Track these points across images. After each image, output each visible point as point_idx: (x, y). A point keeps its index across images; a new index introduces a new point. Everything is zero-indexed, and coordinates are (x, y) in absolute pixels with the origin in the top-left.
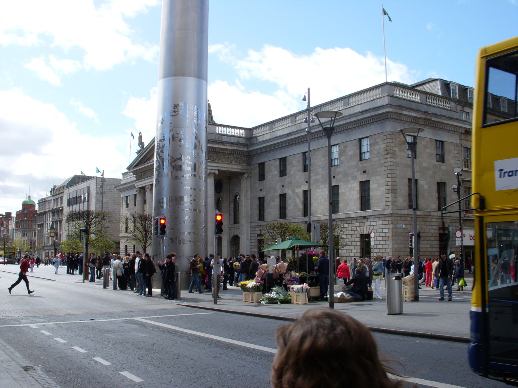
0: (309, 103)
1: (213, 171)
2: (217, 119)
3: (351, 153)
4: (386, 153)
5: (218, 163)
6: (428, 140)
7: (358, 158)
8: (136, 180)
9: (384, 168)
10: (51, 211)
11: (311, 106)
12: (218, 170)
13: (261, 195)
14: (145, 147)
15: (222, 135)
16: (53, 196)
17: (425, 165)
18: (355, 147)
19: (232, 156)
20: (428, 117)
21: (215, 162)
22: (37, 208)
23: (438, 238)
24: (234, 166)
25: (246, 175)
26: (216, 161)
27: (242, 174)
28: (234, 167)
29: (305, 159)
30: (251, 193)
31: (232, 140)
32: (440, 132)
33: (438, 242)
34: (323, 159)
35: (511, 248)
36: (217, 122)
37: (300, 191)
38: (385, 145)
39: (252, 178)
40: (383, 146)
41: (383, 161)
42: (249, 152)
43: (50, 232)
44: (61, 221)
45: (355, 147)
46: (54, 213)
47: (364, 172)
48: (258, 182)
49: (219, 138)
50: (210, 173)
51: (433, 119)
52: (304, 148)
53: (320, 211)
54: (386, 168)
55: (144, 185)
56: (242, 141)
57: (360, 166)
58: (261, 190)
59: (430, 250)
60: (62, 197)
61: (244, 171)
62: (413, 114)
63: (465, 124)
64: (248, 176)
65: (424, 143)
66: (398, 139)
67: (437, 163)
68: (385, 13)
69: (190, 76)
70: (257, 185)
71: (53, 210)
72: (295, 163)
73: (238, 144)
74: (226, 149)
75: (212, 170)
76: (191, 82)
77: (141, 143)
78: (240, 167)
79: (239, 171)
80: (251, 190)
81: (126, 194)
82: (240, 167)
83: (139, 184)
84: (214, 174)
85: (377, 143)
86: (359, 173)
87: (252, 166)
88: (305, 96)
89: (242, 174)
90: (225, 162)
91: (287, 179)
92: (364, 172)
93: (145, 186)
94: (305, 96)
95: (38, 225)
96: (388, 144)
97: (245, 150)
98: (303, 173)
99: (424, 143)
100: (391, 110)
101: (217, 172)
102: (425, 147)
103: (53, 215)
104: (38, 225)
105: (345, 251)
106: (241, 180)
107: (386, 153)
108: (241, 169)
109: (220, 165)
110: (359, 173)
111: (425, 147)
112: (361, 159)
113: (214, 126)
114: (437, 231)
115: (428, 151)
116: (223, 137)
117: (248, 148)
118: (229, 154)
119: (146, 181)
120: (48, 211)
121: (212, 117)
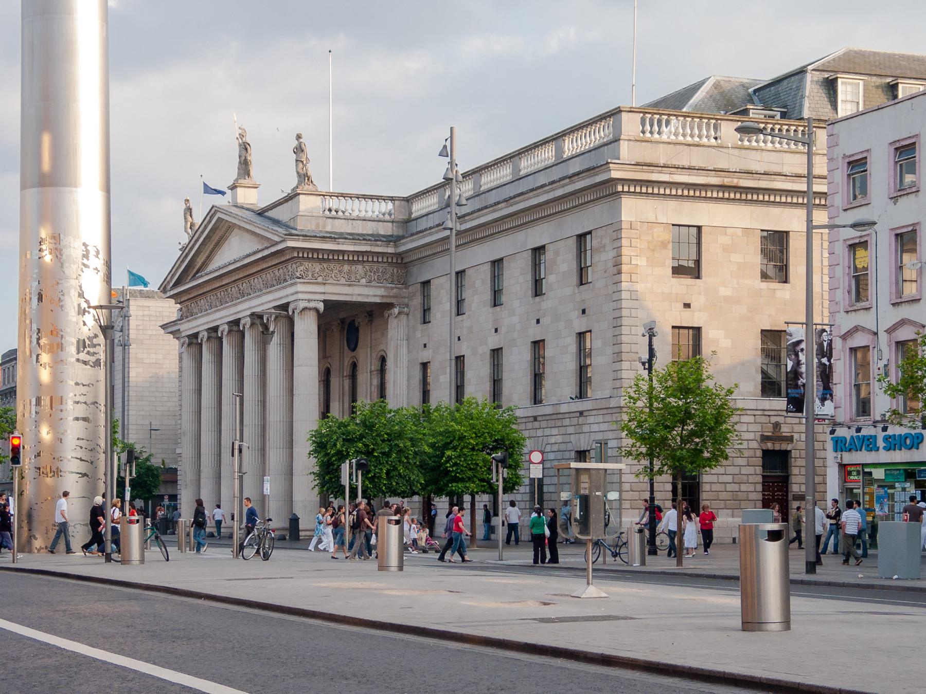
1: (312, 305)
6: (739, 232)
7: (574, 280)
12: (325, 301)
13: (425, 356)
17: (724, 291)
19: (360, 267)
23: (760, 461)
24: (366, 291)
25: (396, 310)
26: (320, 280)
27: (390, 306)
28: (364, 292)
29: (536, 265)
30: (409, 352)
33: (759, 470)
34: (521, 280)
35: (872, 484)
37: (485, 350)
42: (400, 255)
47: (584, 311)
48: (420, 327)
49: (324, 226)
52: (576, 224)
53: (515, 397)
55: (196, 331)
56: (385, 229)
58: (425, 346)
59: (730, 487)
61: (388, 301)
64: (399, 313)
65: (724, 240)
67: (764, 285)
70: (418, 334)
72: (478, 284)
73: (376, 238)
74: (343, 252)
75: (309, 301)
79: (378, 300)
81: (484, 253)
84: (317, 310)
89: (384, 307)
90: (343, 281)
91: (547, 303)
94: (445, 147)
97: (390, 250)
98: (491, 310)
99: (724, 240)
101: (321, 306)
102: (727, 249)
105: (714, 479)
108: (383, 296)
109: (328, 289)
111: (727, 249)
114: (754, 445)
115: (736, 258)
117: (396, 246)
119: (200, 321)
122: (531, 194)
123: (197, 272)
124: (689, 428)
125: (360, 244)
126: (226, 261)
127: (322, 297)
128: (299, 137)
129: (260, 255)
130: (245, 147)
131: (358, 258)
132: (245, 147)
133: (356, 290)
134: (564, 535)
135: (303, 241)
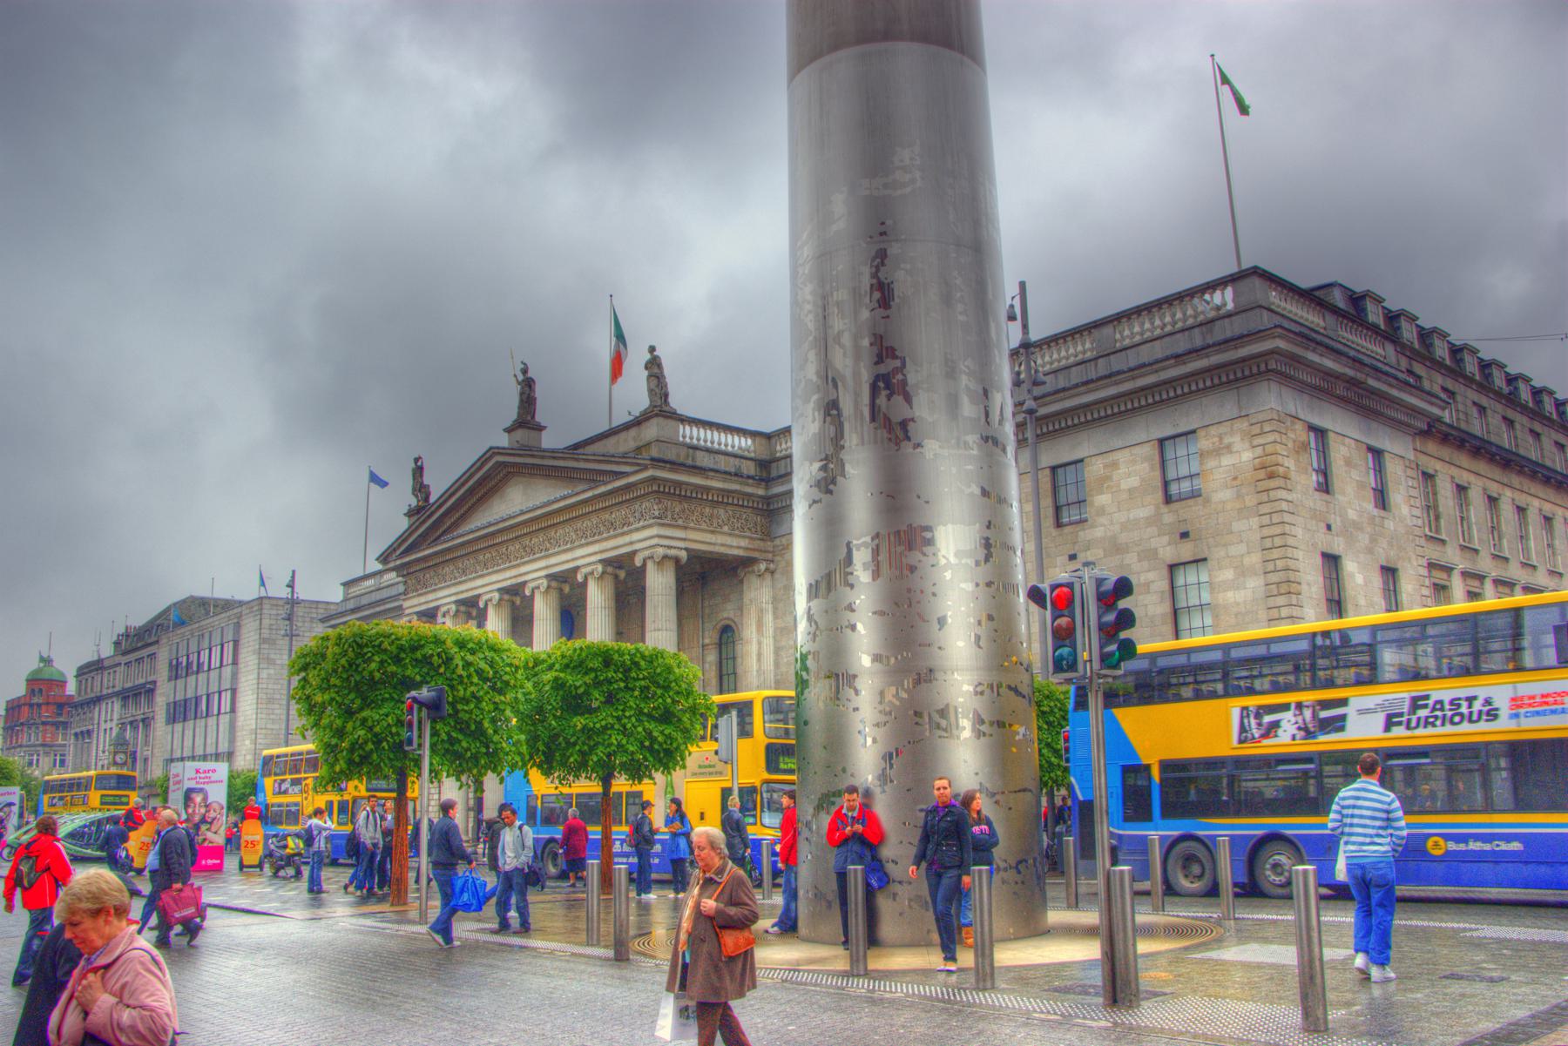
0: (1025, 327)
1: (672, 552)
2: (677, 402)
3: (1134, 482)
4: (1262, 474)
5: (686, 528)
7: (1160, 495)
8: (405, 593)
9: (1254, 522)
10: (117, 694)
11: (1034, 336)
14: (432, 500)
15: (695, 448)
16: (124, 653)
18: (1146, 465)
20: (1359, 376)
21: (678, 527)
22: (71, 688)
25: (763, 566)
26: (680, 522)
27: (746, 563)
30: (776, 617)
31: (723, 464)
32: (1374, 425)
36: (682, 410)
38: (1259, 451)
39: (777, 576)
40: (1247, 456)
41: (1251, 500)
42: (767, 499)
43: (116, 753)
44: (147, 722)
45: (1146, 465)
46: (125, 698)
50: (665, 557)
51: (1371, 382)
54: (1266, 520)
57: (1168, 518)
60: (152, 656)
61: (756, 555)
62: (1329, 363)
63: (1432, 404)
66: (1291, 435)
68: (1225, 80)
69: (902, 39)
71: (124, 690)
74: (708, 489)
75: (670, 547)
76: (106, 664)
77: (421, 489)
78: (744, 543)
79: (741, 553)
80: (775, 609)
82: (744, 543)
83: (415, 601)
84: (677, 560)
85: (1229, 448)
86: (1165, 539)
87: (777, 542)
88: (1012, 306)
89: (746, 563)
90: (704, 526)
92: (1185, 535)
93: (437, 608)
95: (76, 735)
96: (1269, 449)
97: (761, 492)
100: (1281, 344)
101: (683, 555)
103: (124, 706)
104: (76, 735)
106: (741, 582)
107: (1262, 474)
108: (747, 549)
110: (1165, 539)
112: (1168, 499)
113: (672, 423)
116: (699, 454)
117: (767, 488)
118: (715, 504)
120: (109, 696)
121: (667, 395)
122: (1082, 389)
123: (444, 533)
124: (451, 789)
125: (731, 481)
126: (497, 517)
127: (599, 557)
128: (652, 349)
129: (562, 504)
130: (528, 384)
131: (723, 499)
132: (528, 384)
133: (720, 539)
134: (1277, 879)
135: (671, 470)
